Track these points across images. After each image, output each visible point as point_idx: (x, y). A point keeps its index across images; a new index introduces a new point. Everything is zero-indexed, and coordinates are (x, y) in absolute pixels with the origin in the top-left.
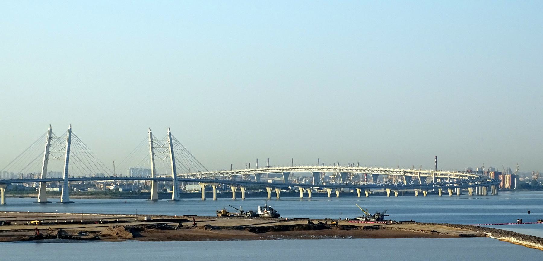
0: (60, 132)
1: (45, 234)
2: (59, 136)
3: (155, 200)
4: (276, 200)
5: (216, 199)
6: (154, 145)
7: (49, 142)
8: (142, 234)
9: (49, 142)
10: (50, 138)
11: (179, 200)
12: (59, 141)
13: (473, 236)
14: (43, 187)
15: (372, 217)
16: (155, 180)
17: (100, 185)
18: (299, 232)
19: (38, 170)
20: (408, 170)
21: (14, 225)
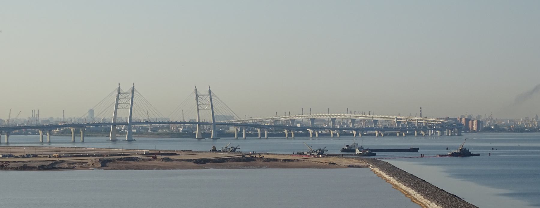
0: (126, 88)
1: (29, 164)
2: (125, 92)
3: (199, 139)
4: (291, 139)
5: (245, 138)
6: (199, 98)
7: (118, 96)
8: (56, 166)
9: (118, 96)
10: (119, 93)
11: (216, 139)
12: (125, 96)
13: (359, 167)
14: (130, 130)
15: (315, 152)
16: (199, 125)
17: (173, 127)
18: (231, 163)
19: (109, 117)
20: (399, 117)
21: (40, 157)
